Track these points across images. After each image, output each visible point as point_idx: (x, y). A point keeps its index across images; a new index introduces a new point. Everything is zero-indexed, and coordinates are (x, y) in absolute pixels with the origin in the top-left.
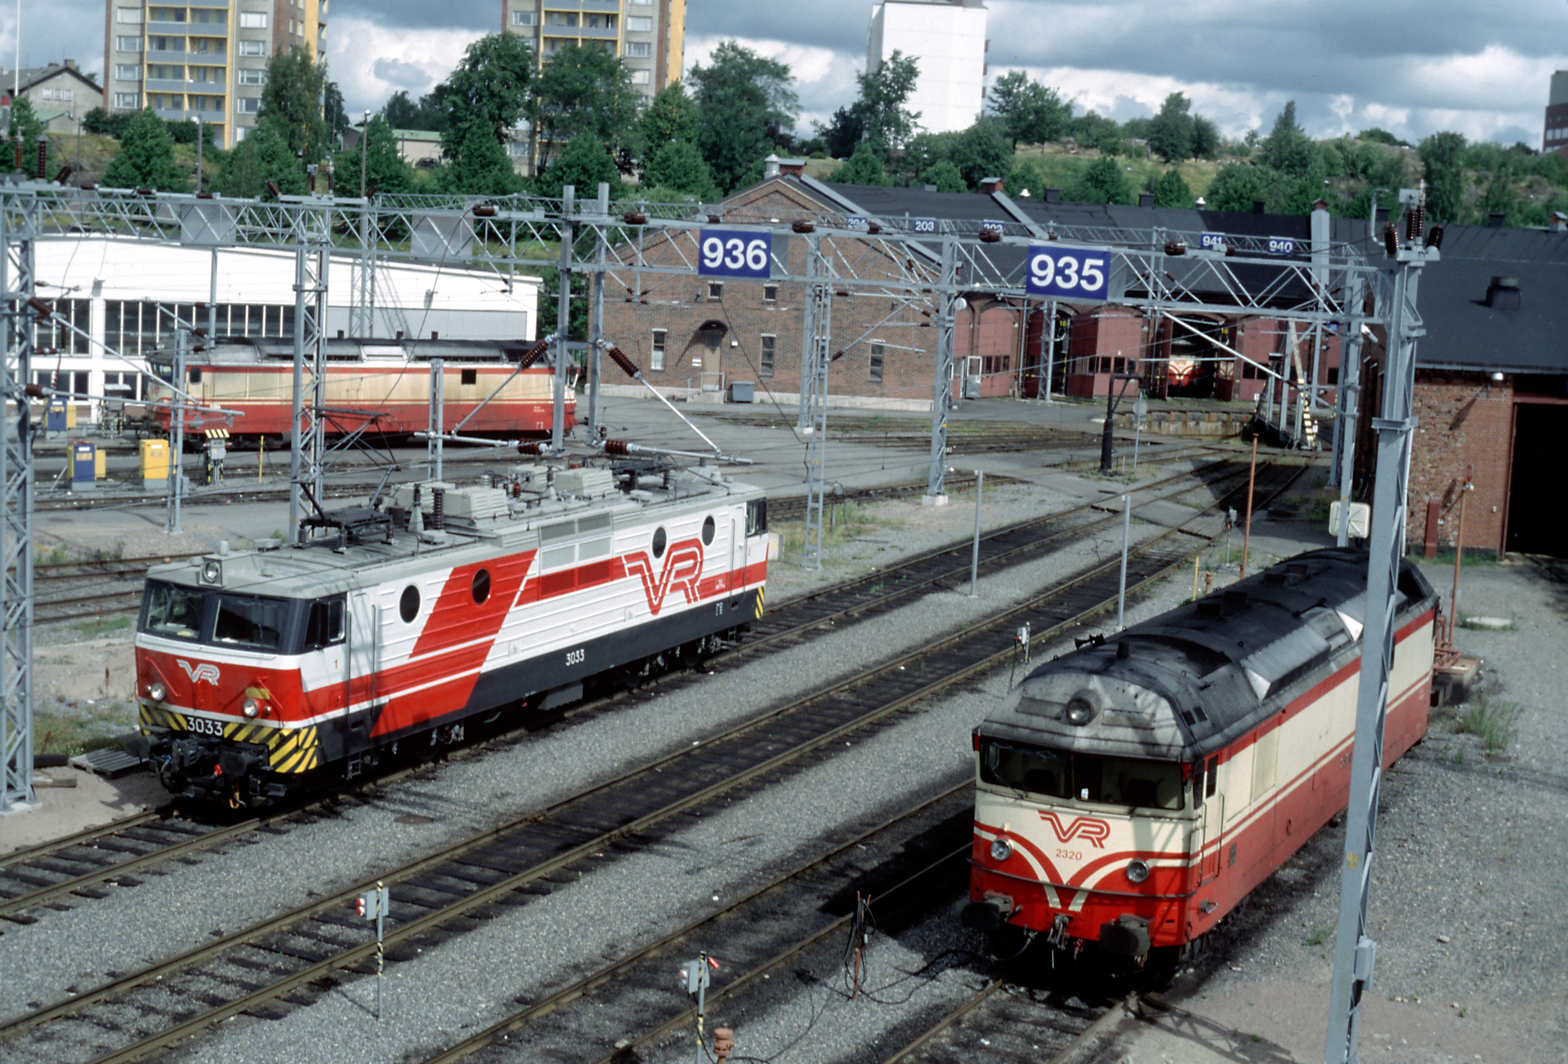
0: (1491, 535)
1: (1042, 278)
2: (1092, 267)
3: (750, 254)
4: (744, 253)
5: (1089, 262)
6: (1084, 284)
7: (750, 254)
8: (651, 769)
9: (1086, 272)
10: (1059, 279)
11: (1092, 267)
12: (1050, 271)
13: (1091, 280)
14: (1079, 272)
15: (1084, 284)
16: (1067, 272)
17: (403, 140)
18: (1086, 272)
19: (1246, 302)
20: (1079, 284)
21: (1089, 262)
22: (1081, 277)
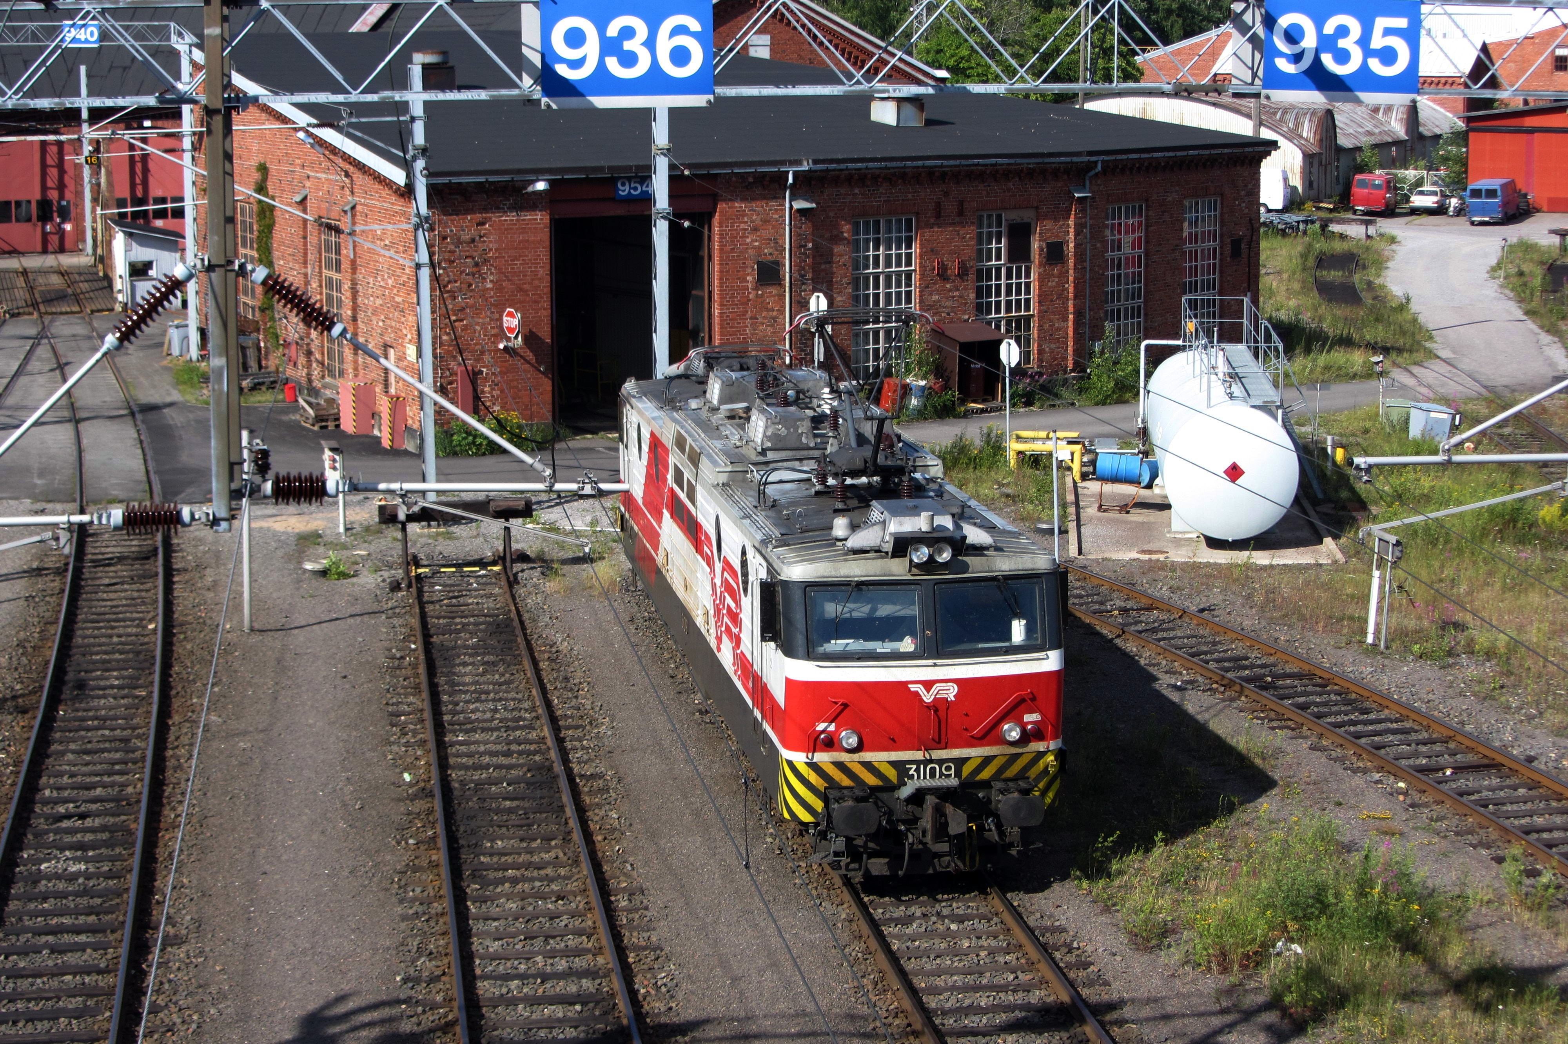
0: (133, 259)
1: (576, 64)
2: (1388, 32)
3: (665, 45)
4: (650, 44)
5: (1381, 23)
6: (1375, 65)
7: (665, 45)
8: (634, 646)
9: (1378, 42)
10: (612, 64)
11: (1388, 32)
12: (591, 48)
13: (1388, 56)
14: (1364, 41)
15: (1375, 65)
16: (628, 45)
17: (523, 571)
18: (1378, 42)
19: (850, 77)
20: (1364, 66)
21: (1381, 23)
22: (1368, 53)
